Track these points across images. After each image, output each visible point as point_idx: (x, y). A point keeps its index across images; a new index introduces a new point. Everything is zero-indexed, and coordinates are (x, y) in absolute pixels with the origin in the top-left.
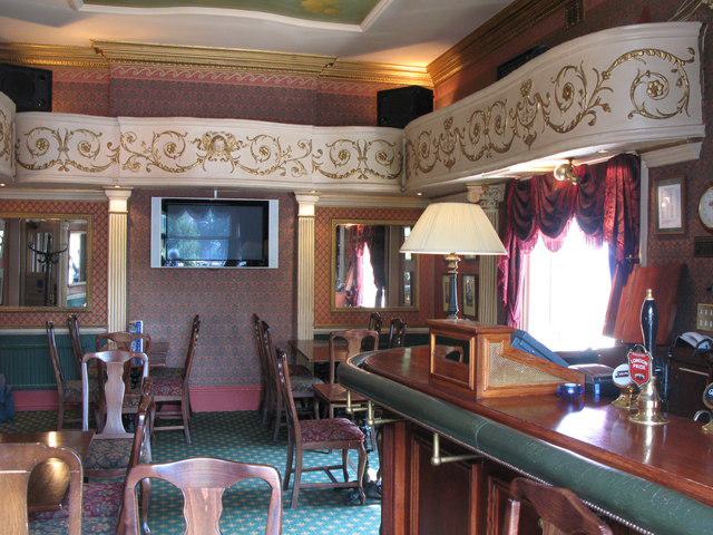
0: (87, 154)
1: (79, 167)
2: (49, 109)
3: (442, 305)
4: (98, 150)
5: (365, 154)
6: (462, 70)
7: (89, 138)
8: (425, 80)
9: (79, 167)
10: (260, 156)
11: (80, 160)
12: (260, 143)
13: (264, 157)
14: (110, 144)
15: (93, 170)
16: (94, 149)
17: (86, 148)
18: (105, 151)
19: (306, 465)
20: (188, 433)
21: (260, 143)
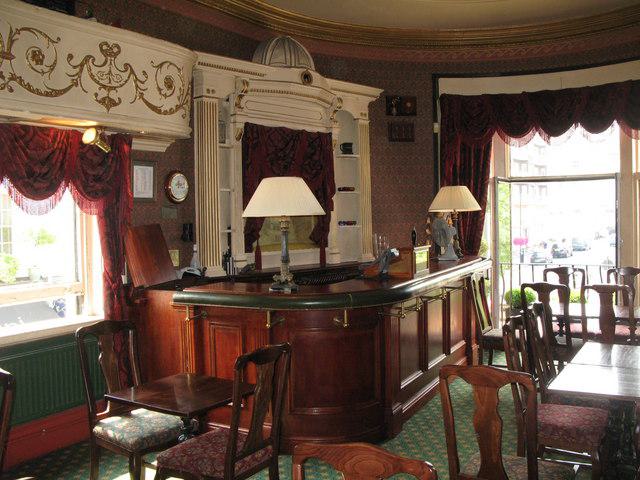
0: (38, 67)
1: (29, 87)
2: (251, 61)
3: (442, 130)
4: (55, 64)
5: (10, 48)
6: (209, 421)
7: (41, 43)
8: (300, 442)
9: (29, 87)
10: (165, 91)
11: (29, 77)
12: (166, 71)
13: (169, 92)
14: (70, 57)
15: (47, 94)
16: (48, 61)
17: (37, 57)
18: (64, 69)
19: (8, 391)
20: (354, 171)
21: (166, 71)
